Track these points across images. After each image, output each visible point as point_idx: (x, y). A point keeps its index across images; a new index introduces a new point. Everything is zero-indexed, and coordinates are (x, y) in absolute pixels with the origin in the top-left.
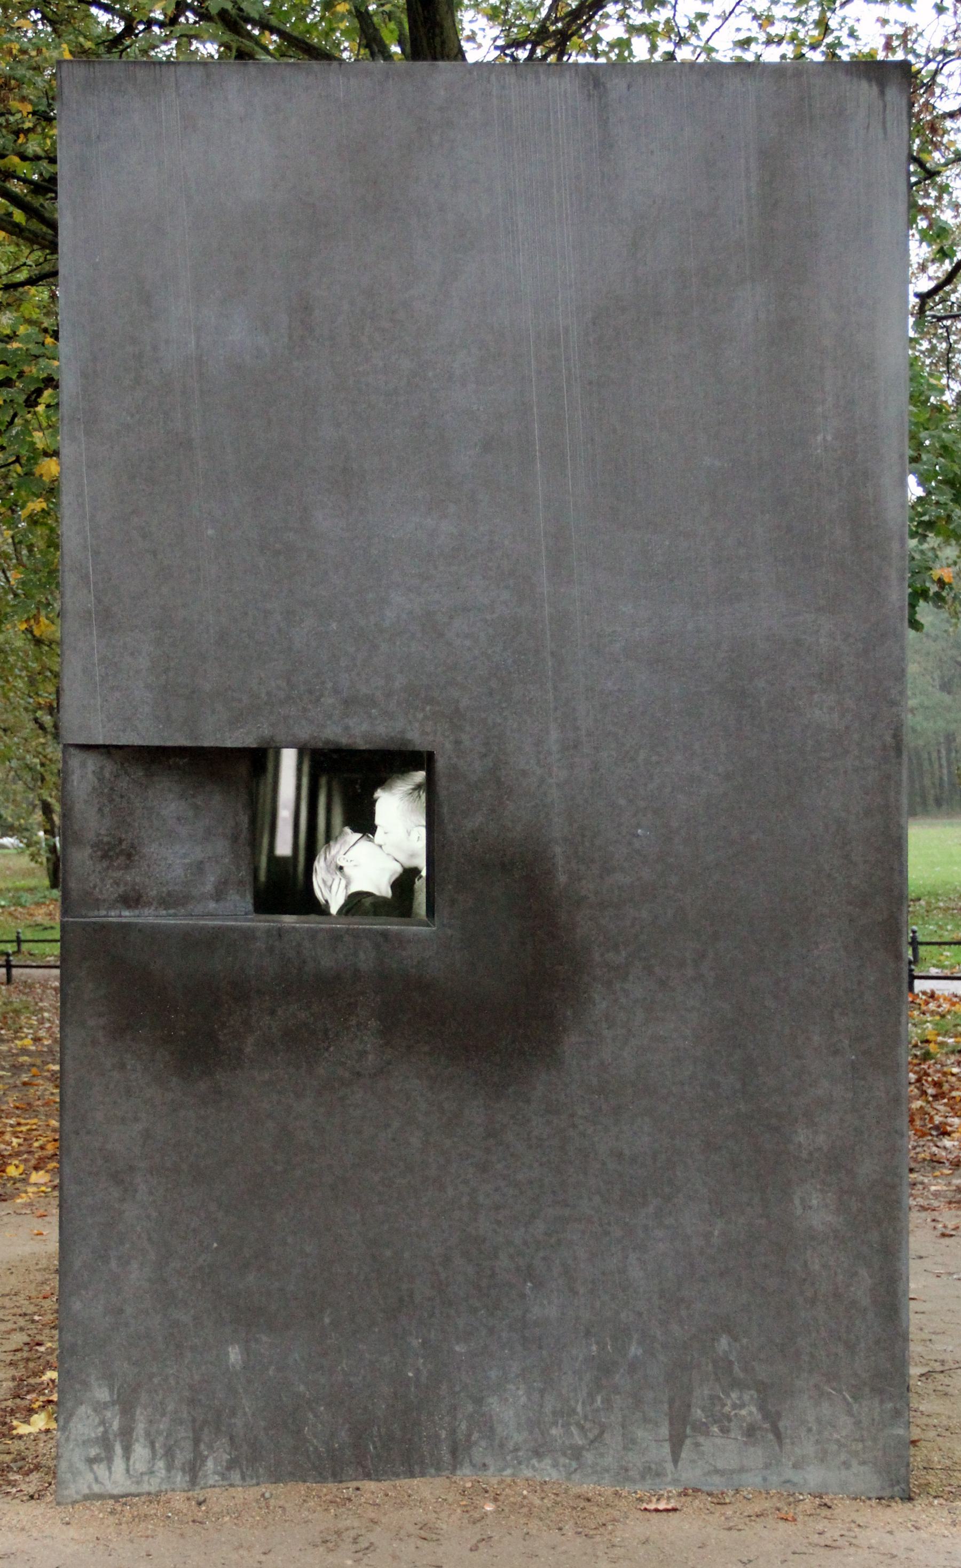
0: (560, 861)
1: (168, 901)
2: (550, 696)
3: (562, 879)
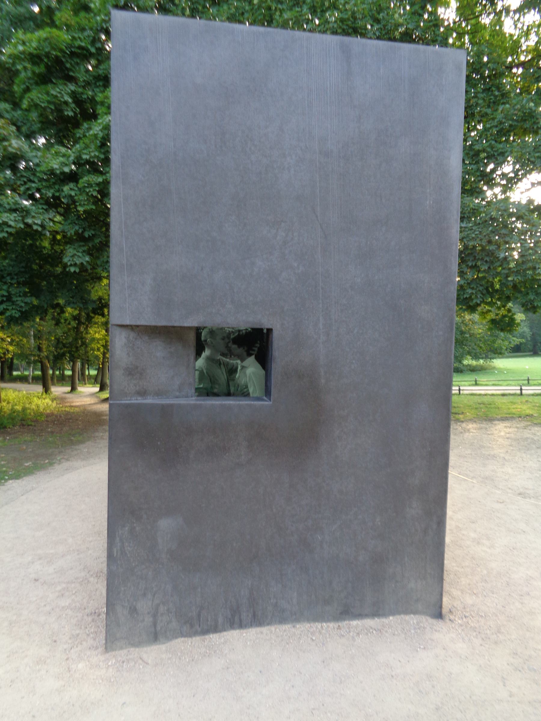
0: (322, 373)
1: (158, 394)
2: (321, 306)
3: (323, 381)
